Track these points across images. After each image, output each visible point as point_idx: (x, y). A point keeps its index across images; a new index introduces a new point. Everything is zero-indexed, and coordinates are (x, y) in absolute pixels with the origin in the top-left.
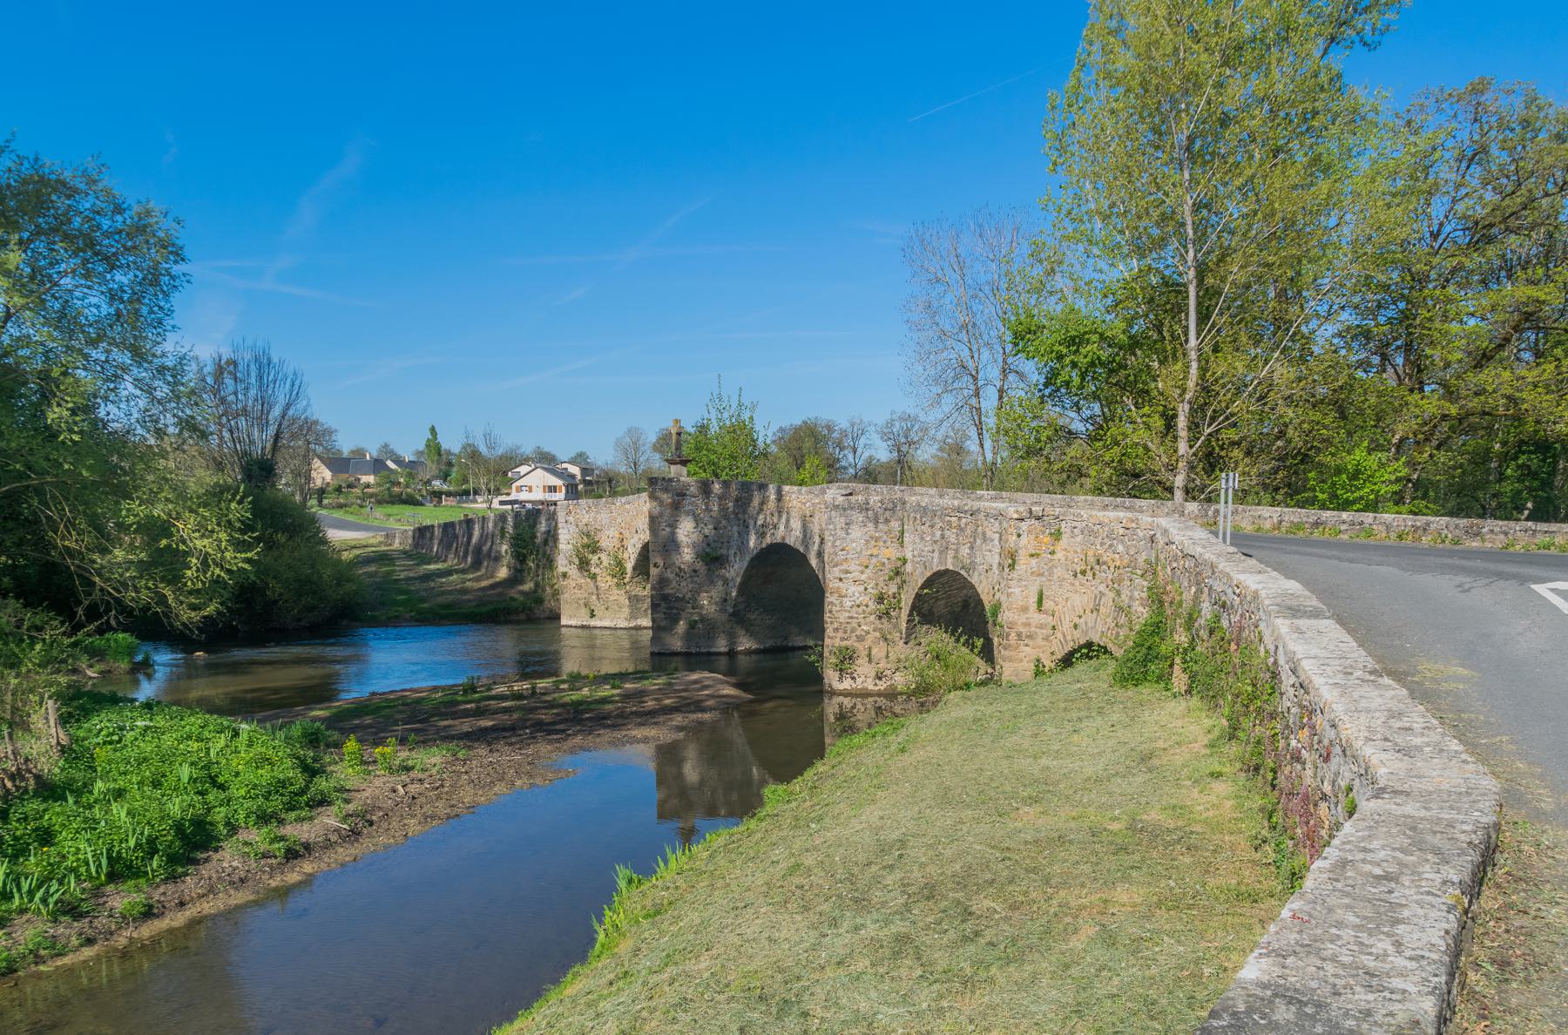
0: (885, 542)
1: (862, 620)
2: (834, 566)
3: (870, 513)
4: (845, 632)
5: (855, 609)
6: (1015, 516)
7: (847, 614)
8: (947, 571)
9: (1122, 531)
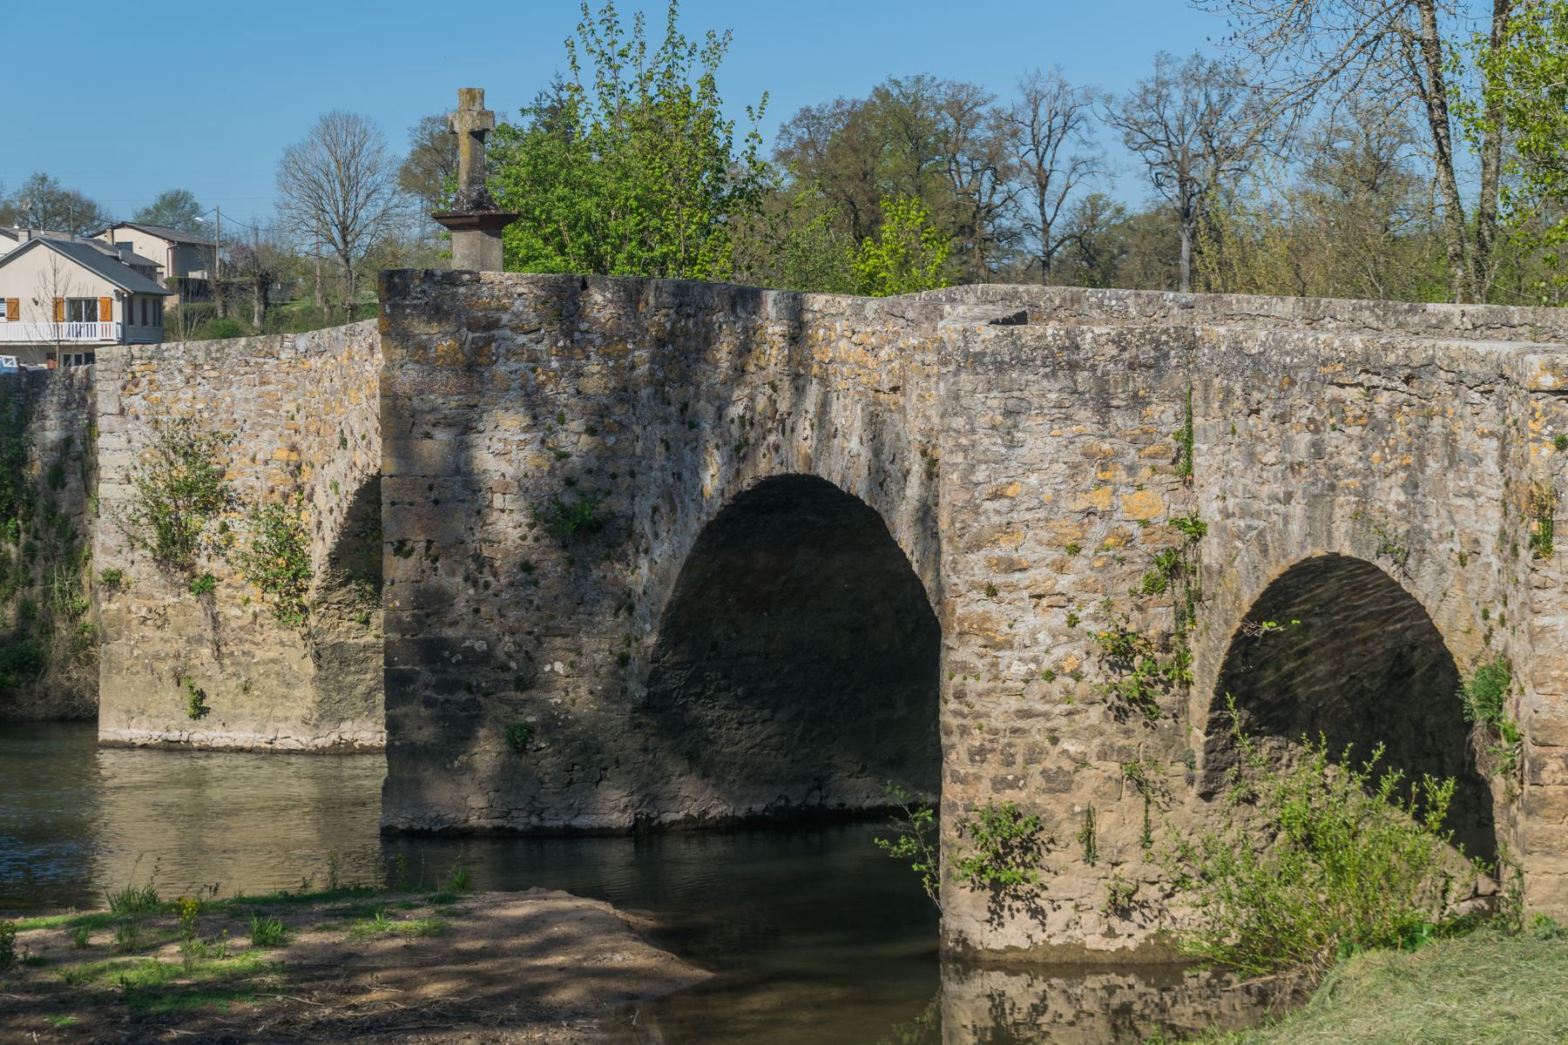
0: (1131, 469)
2: (970, 549)
3: (1082, 376)
7: (1014, 704)
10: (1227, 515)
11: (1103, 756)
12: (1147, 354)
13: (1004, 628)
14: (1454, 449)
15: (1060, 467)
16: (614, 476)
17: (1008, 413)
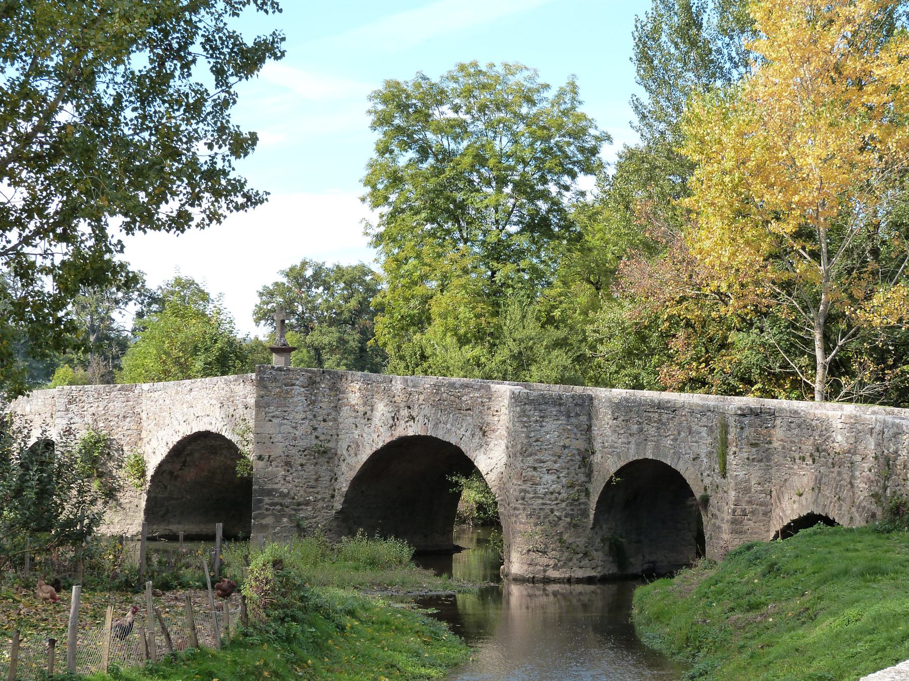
0: (575, 434)
1: (555, 507)
2: (528, 456)
3: (562, 408)
5: (548, 496)
7: (540, 501)
12: (580, 402)
13: (538, 479)
14: (690, 430)
16: (332, 435)
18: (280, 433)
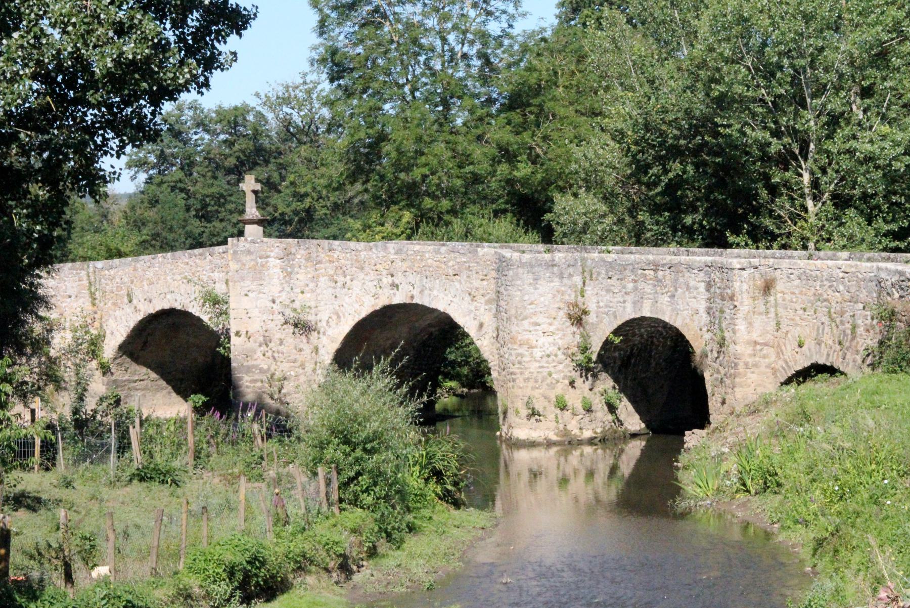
1: (552, 370)
4: (536, 381)
6: (739, 266)
7: (538, 364)
8: (643, 319)
9: (841, 275)
10: (599, 307)
11: (563, 379)
15: (550, 295)
17: (535, 279)
18: (256, 307)
